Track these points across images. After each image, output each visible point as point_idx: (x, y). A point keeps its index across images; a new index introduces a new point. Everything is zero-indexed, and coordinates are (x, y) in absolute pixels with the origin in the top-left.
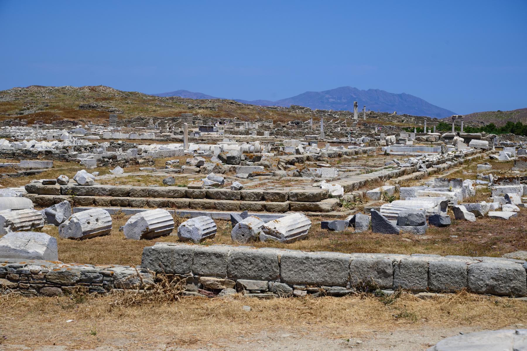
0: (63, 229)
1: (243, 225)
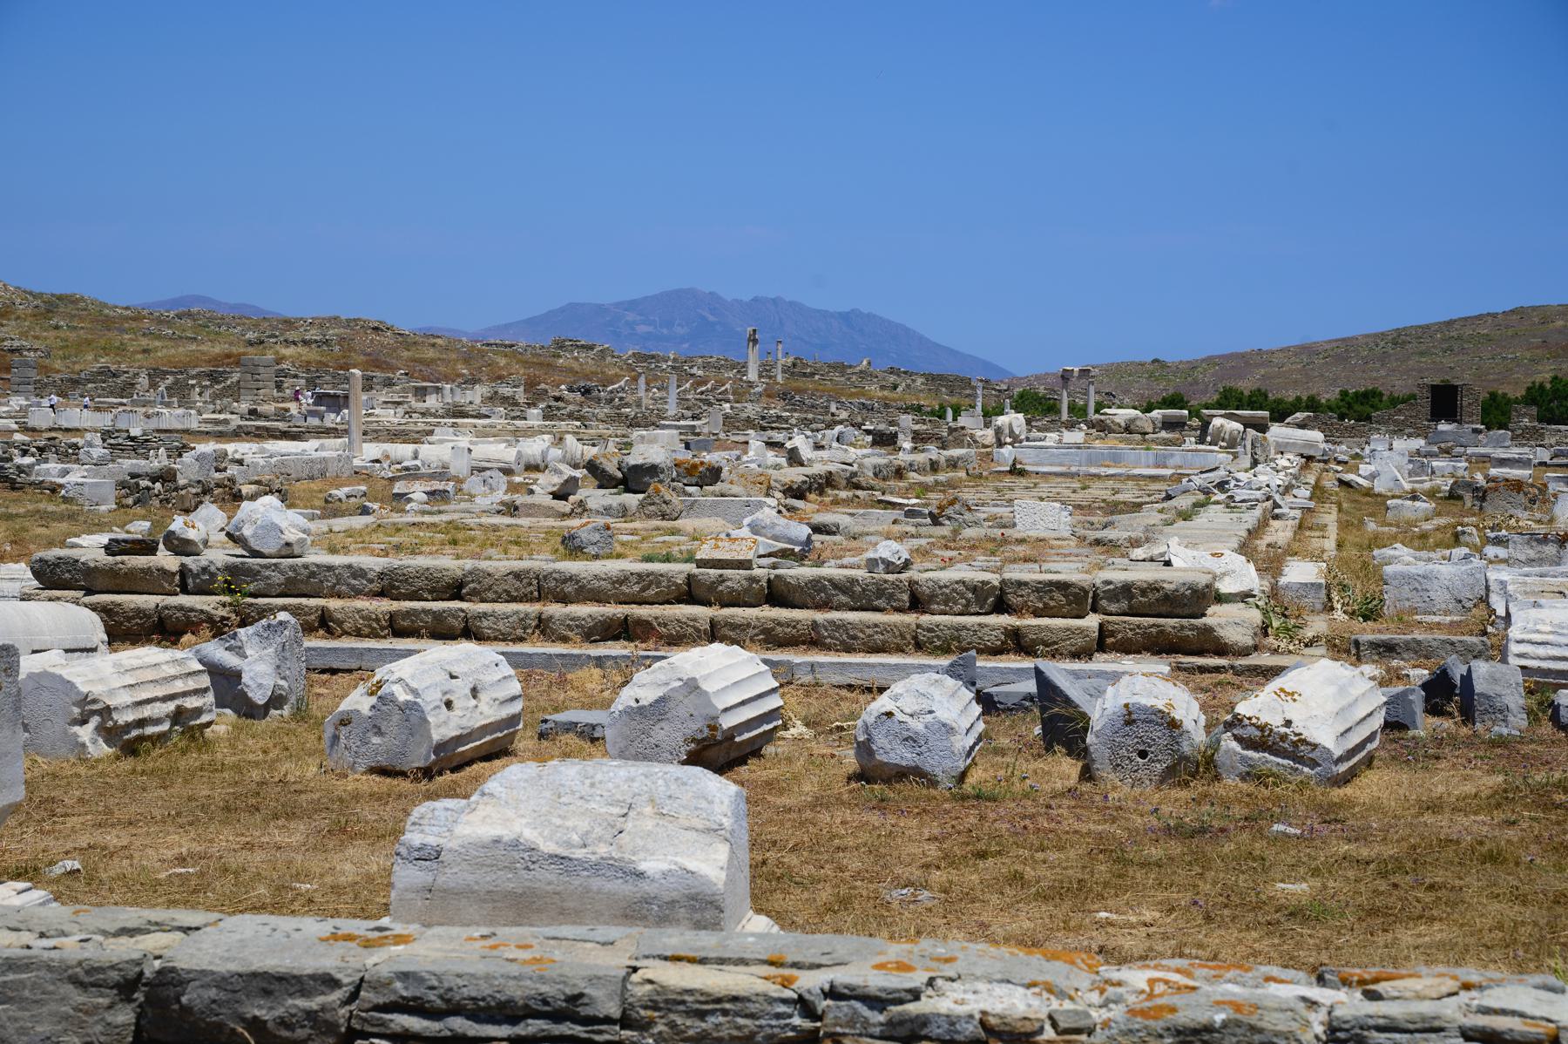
0: (344, 731)
1: (1144, 709)
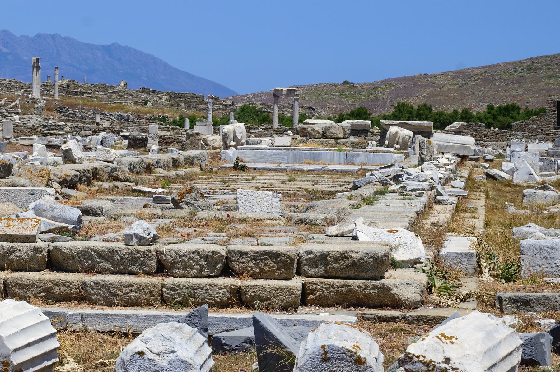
1: (337, 350)
